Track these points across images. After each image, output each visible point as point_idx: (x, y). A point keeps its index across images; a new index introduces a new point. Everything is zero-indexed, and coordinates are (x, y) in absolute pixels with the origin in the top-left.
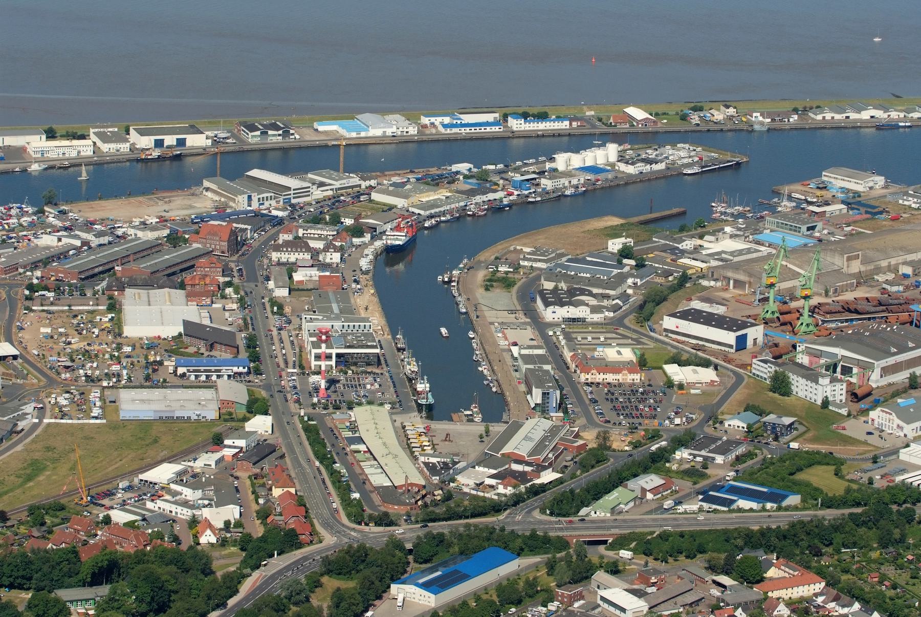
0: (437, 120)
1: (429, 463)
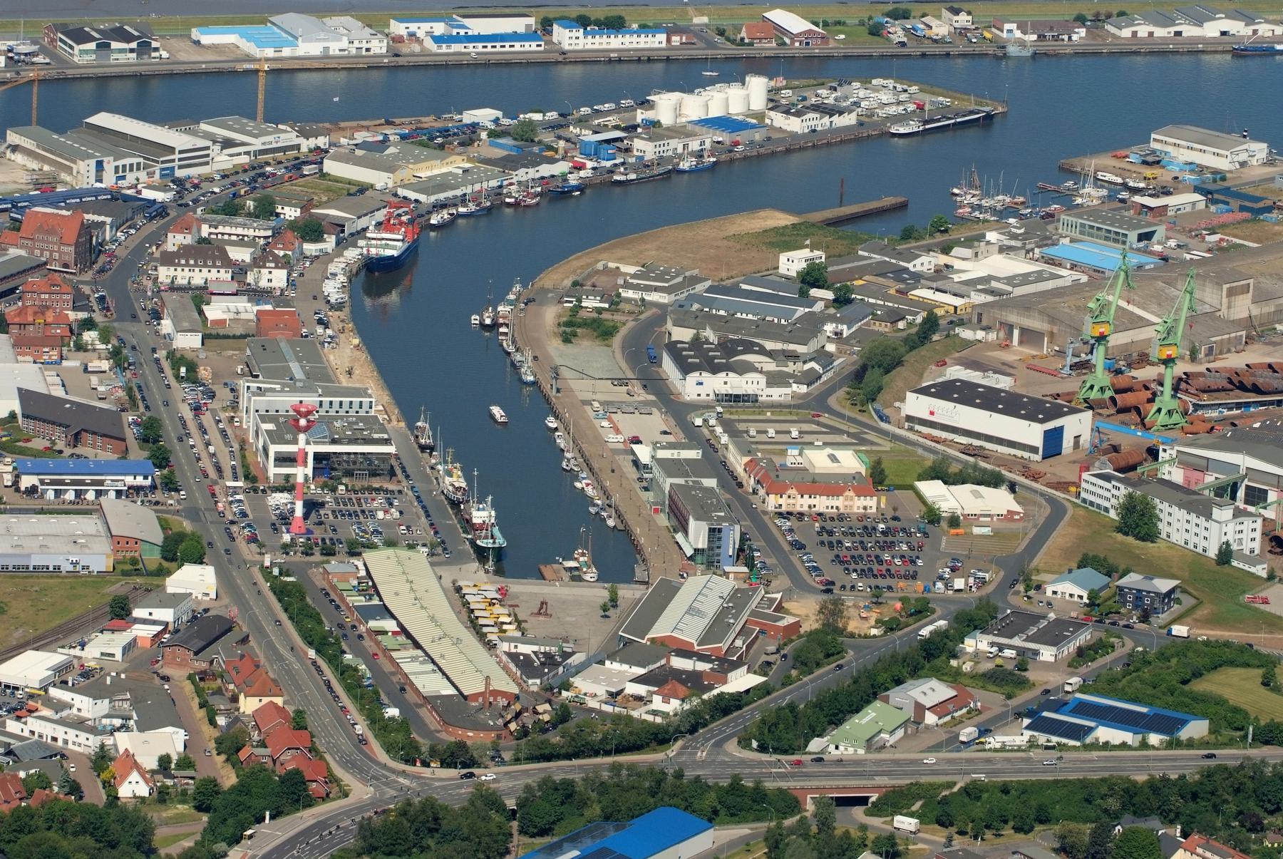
0: (421, 29)
1: (517, 655)
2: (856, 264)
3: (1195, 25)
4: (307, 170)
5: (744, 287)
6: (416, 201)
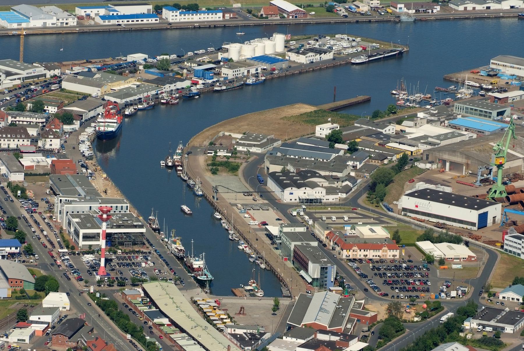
0: (93, 12)
1: (236, 335)
2: (355, 130)
3: (497, 3)
4: (53, 87)
5: (299, 143)
6: (115, 102)
